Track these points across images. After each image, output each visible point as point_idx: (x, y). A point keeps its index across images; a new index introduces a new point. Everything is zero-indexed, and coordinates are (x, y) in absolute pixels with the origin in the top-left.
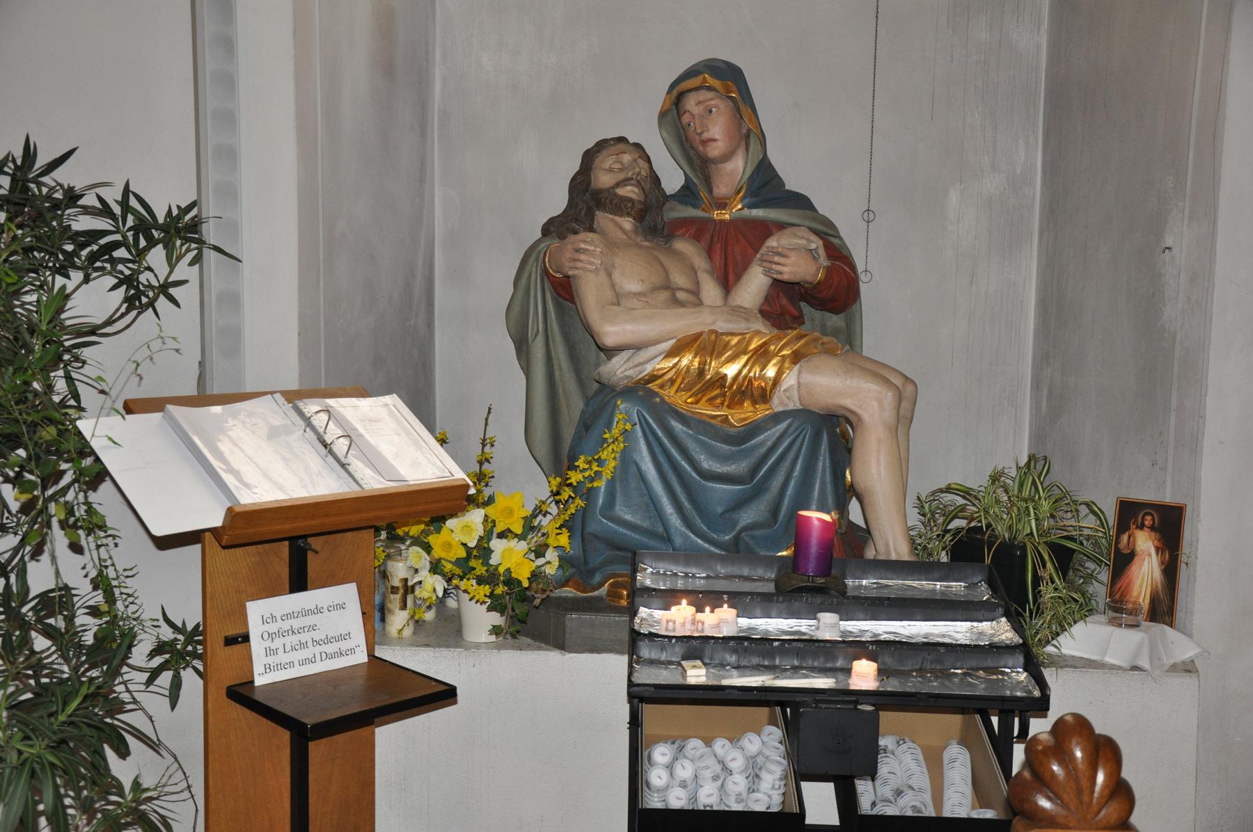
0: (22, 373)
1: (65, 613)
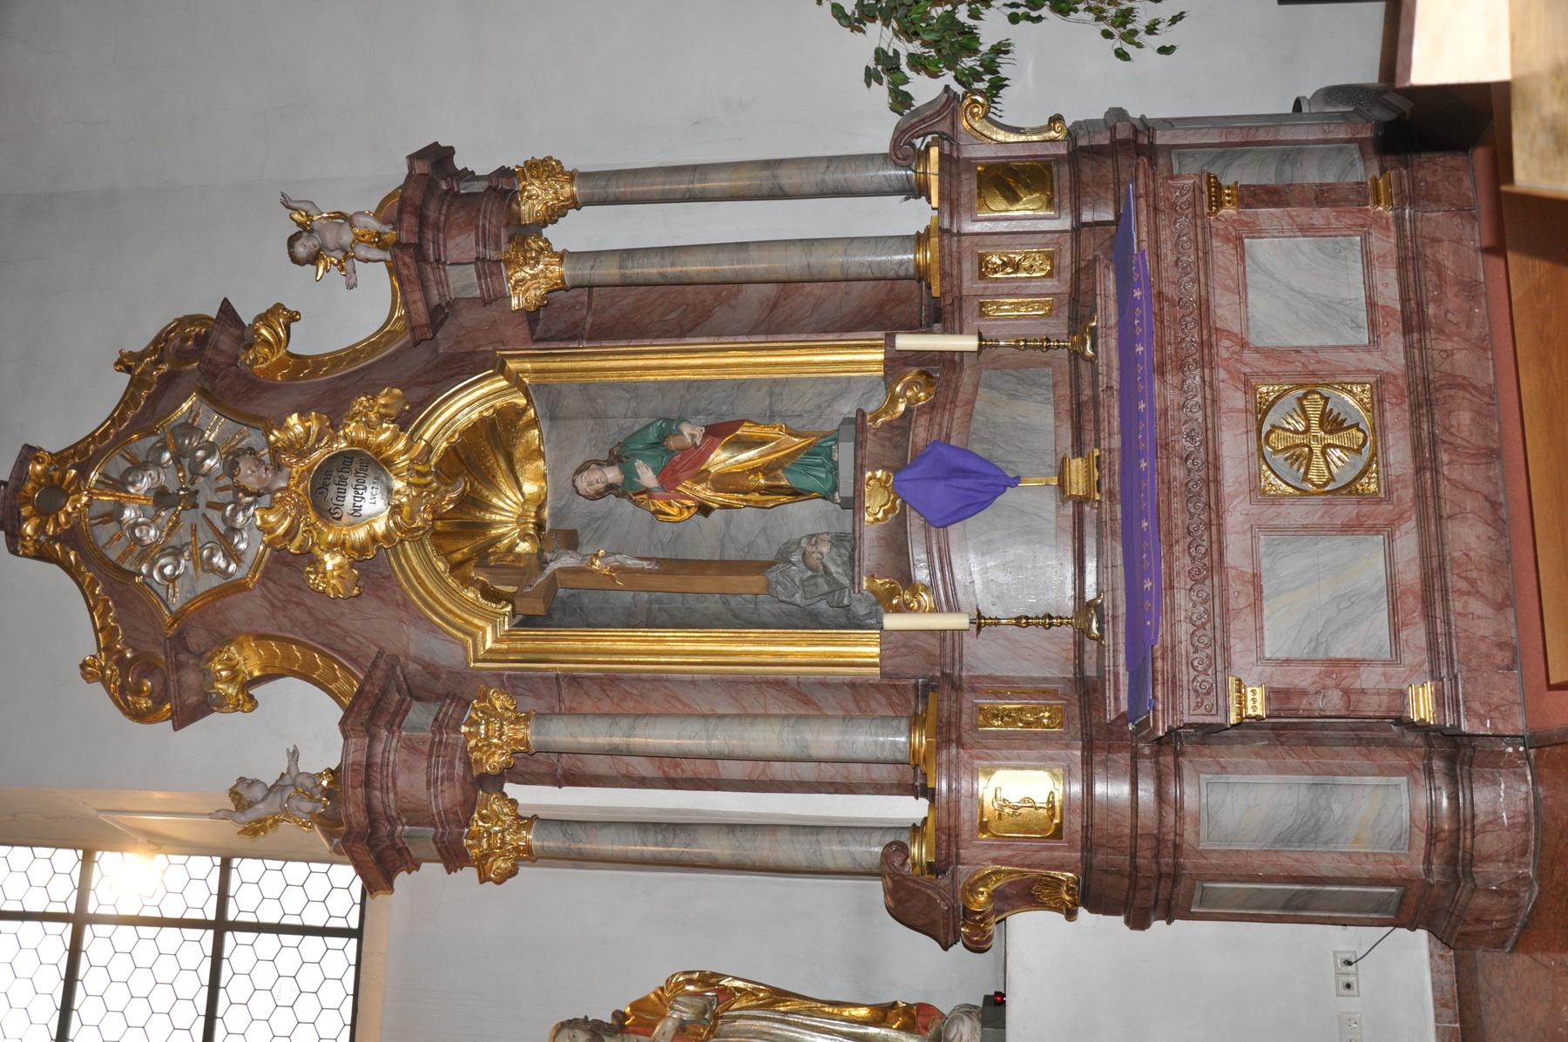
0: (1490, 534)
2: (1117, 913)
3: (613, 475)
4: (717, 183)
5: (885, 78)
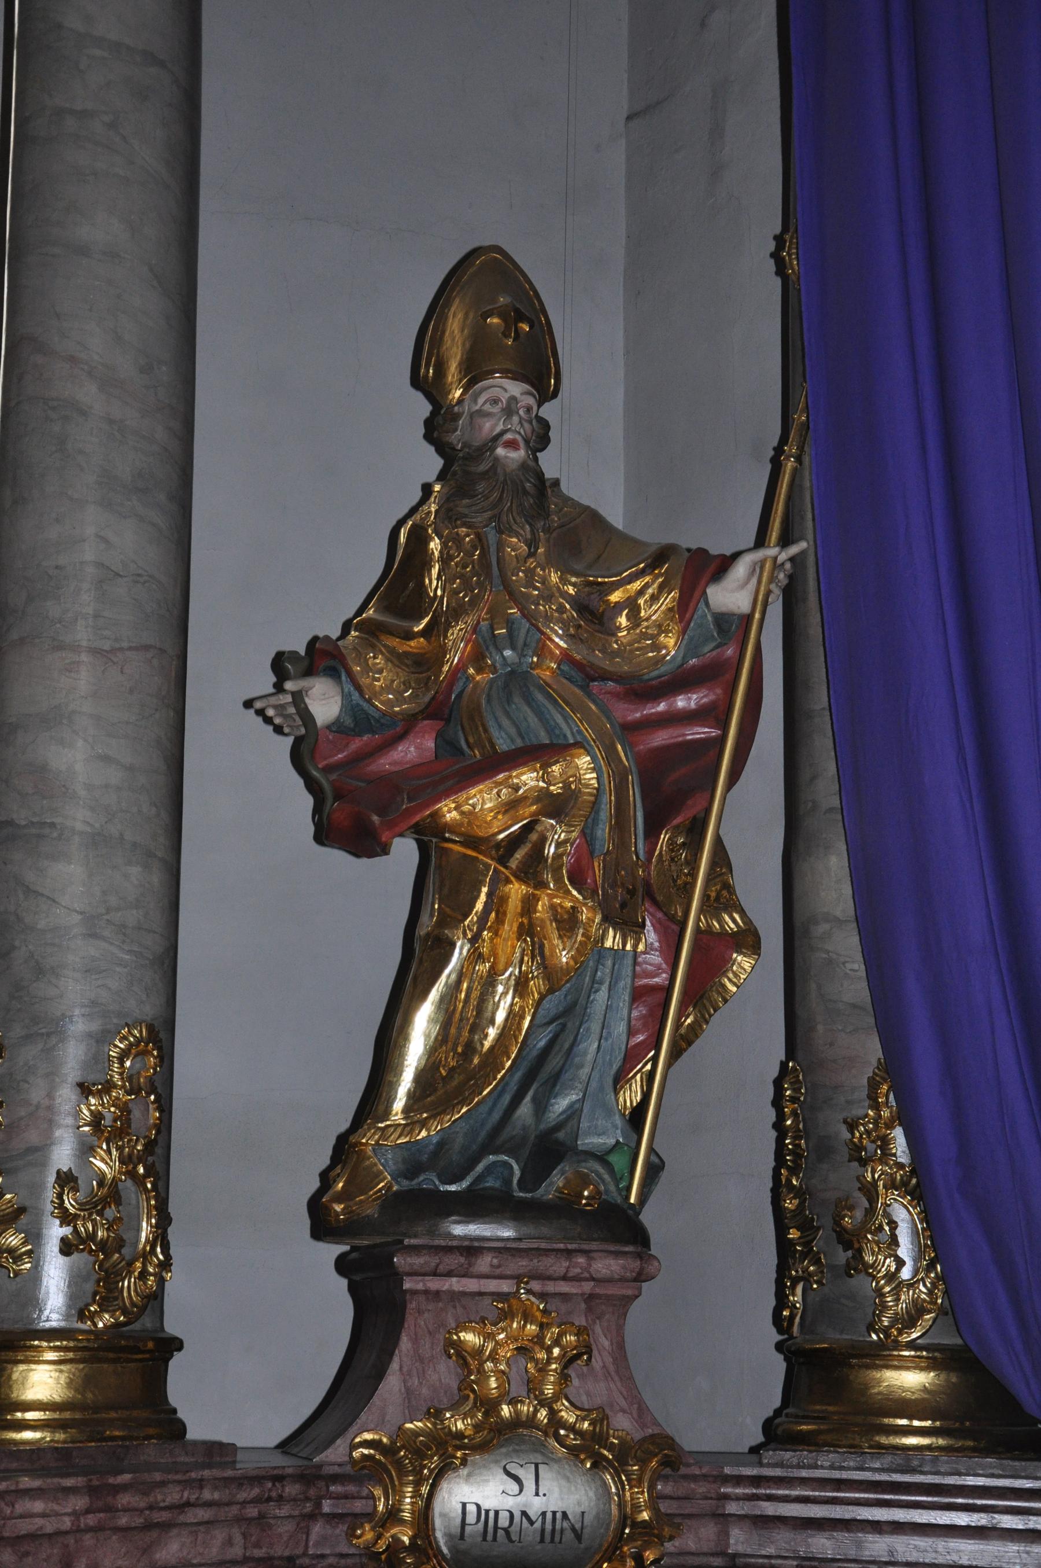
1: (455, 1337)
5: (454, 1358)
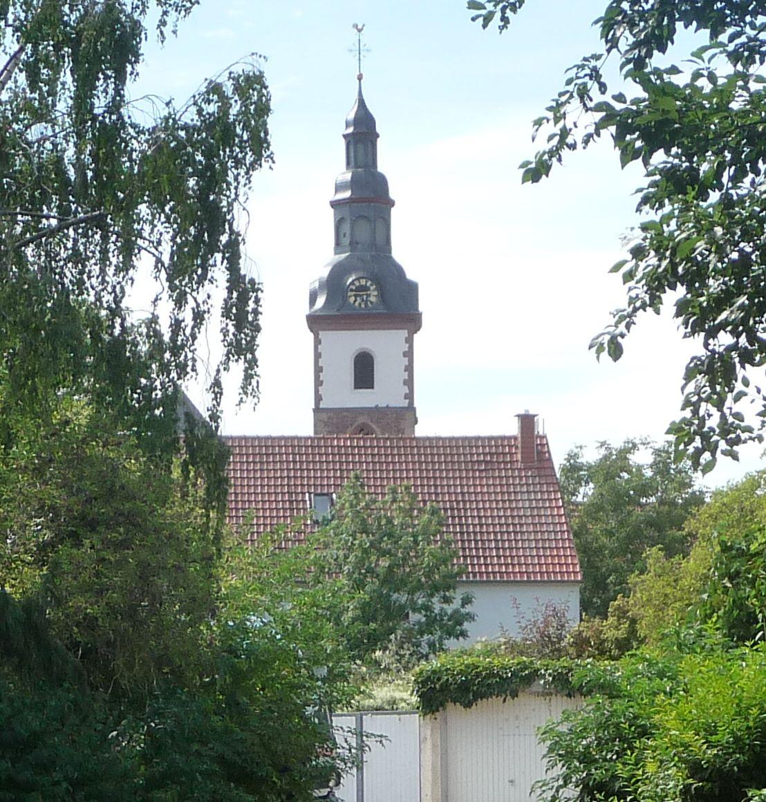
2: (380, 173)
3: (471, 575)
4: (360, 788)
